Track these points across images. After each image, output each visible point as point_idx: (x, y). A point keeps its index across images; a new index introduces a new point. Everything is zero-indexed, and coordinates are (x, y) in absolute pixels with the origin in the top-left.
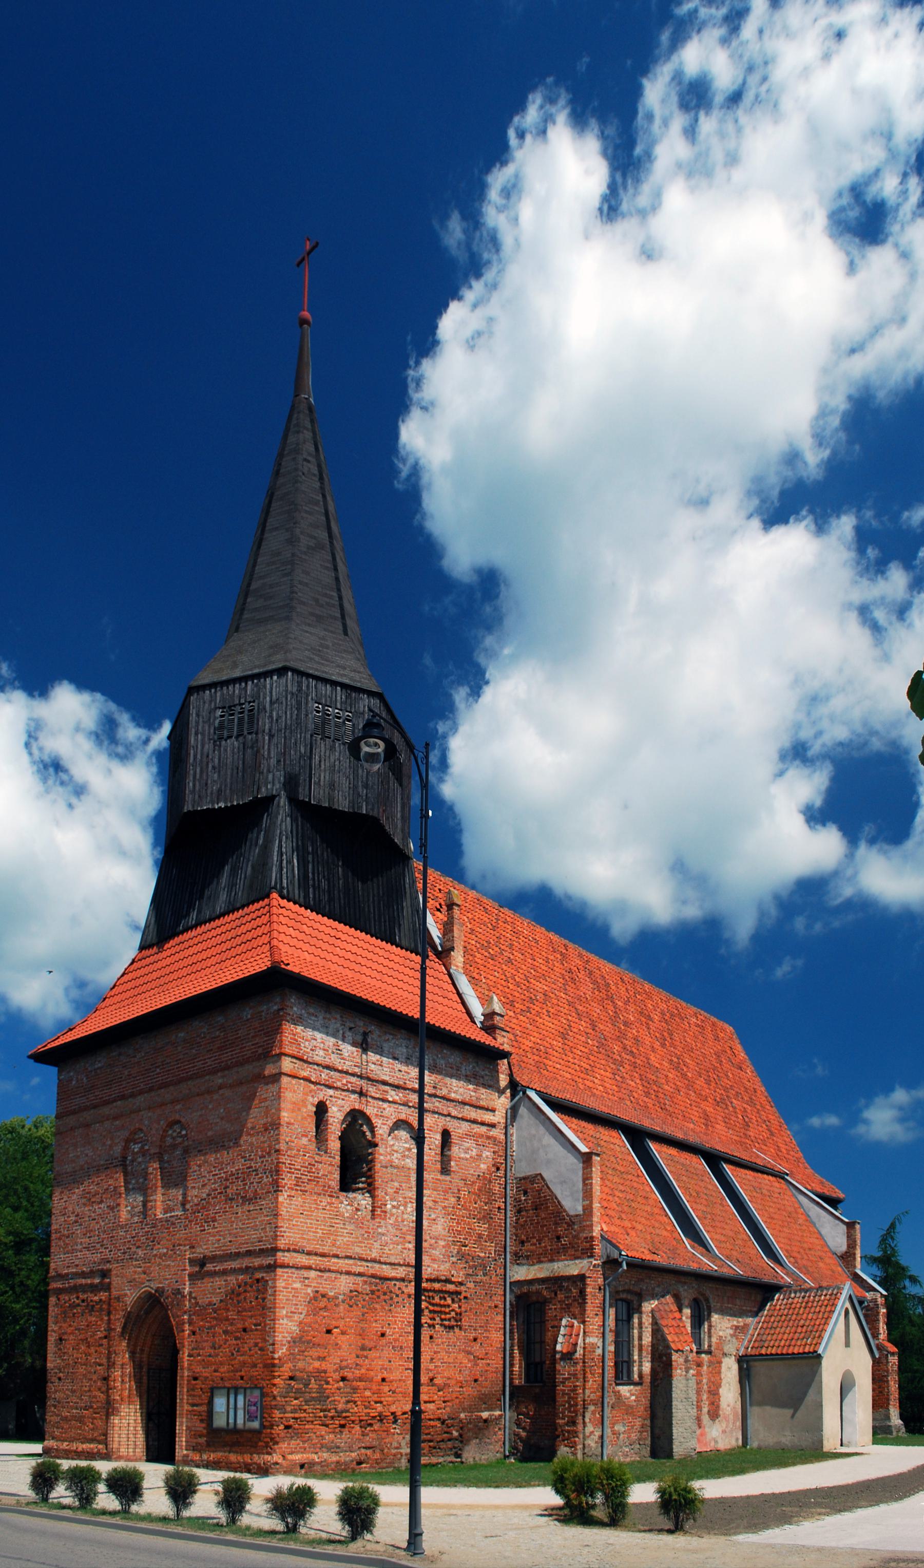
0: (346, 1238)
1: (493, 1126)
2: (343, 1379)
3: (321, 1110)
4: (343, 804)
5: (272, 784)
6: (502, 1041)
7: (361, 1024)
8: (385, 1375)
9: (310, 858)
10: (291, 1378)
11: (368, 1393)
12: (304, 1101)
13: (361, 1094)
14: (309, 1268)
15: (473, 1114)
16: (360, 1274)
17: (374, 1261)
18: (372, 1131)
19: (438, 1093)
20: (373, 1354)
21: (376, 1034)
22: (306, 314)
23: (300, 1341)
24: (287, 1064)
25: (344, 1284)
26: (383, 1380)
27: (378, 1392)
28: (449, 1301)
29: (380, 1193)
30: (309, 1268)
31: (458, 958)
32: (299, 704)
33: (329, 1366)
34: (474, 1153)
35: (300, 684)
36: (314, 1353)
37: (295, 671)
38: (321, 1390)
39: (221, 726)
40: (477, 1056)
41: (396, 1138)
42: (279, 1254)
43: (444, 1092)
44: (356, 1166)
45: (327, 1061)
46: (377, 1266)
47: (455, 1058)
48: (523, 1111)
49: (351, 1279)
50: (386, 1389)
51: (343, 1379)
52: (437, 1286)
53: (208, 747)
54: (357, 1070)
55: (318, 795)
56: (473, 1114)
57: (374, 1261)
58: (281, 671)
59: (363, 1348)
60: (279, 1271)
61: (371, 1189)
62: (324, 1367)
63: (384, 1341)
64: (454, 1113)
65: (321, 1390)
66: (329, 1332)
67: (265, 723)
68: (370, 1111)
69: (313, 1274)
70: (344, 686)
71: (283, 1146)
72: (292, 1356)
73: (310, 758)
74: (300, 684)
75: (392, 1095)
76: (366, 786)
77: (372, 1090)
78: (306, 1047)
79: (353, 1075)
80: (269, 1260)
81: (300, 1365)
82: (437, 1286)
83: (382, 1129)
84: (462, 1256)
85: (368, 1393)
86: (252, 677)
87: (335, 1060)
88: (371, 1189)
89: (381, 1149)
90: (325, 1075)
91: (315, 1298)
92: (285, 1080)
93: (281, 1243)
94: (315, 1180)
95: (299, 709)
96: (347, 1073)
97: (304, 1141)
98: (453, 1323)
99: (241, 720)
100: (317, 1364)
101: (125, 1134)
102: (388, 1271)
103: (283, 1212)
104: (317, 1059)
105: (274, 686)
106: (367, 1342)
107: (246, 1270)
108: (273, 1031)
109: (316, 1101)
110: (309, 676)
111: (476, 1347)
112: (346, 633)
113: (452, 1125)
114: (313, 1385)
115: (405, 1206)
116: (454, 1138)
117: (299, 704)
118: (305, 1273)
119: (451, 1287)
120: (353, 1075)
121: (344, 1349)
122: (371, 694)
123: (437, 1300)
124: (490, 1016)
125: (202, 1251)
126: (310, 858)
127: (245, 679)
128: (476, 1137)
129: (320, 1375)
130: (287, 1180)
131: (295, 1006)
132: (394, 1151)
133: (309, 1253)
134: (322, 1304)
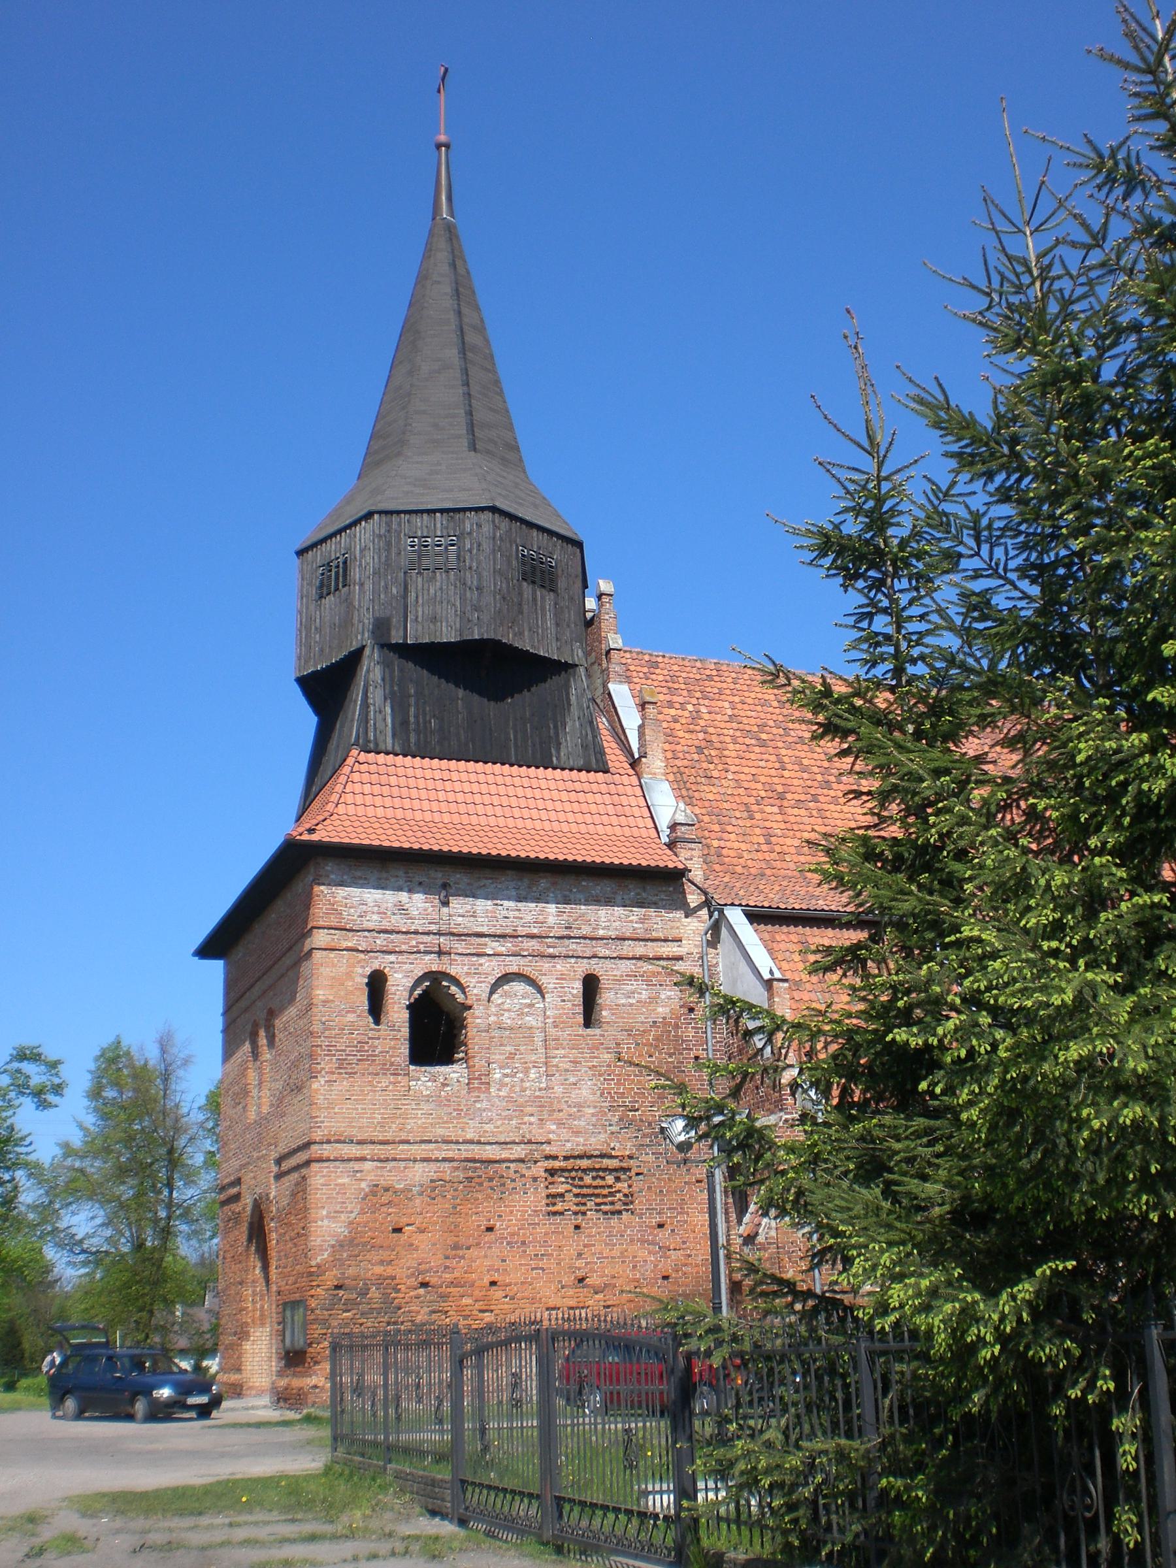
0: (418, 1120)
1: (679, 958)
2: (424, 1285)
3: (377, 985)
4: (448, 635)
5: (361, 636)
6: (692, 860)
7: (438, 876)
8: (496, 1277)
9: (412, 701)
10: (338, 1287)
11: (466, 1301)
12: (349, 975)
13: (440, 953)
14: (363, 1159)
15: (640, 949)
16: (444, 1160)
17: (471, 1142)
18: (463, 989)
19: (575, 933)
20: (474, 1252)
21: (459, 878)
22: (443, 138)
23: (352, 1244)
24: (320, 938)
25: (420, 1173)
26: (493, 1283)
27: (485, 1298)
28: (610, 1179)
29: (479, 1062)
30: (363, 1159)
31: (655, 763)
32: (389, 544)
33: (402, 1270)
34: (644, 995)
35: (389, 524)
36: (375, 1256)
37: (380, 513)
38: (387, 1301)
39: (321, 586)
40: (657, 884)
41: (506, 995)
42: (314, 1147)
43: (586, 930)
44: (437, 1030)
45: (386, 925)
46: (476, 1147)
47: (605, 887)
48: (724, 932)
49: (433, 1166)
50: (497, 1293)
51: (424, 1285)
52: (585, 1163)
53: (312, 607)
54: (434, 928)
55: (416, 633)
56: (640, 949)
57: (471, 1142)
58: (369, 516)
59: (456, 1247)
60: (315, 1166)
61: (466, 1060)
62: (390, 1271)
63: (489, 1237)
64: (603, 952)
65: (387, 1301)
66: (398, 1230)
67: (356, 574)
68: (453, 971)
69: (368, 1165)
70: (442, 511)
71: (317, 1027)
72: (336, 1261)
73: (405, 596)
74: (389, 524)
75: (492, 946)
76: (476, 608)
77: (460, 947)
78: (350, 916)
79: (428, 933)
80: (302, 1157)
81: (351, 1272)
82: (585, 1163)
83: (477, 989)
84: (626, 1123)
85: (466, 1301)
86: (344, 529)
87: (398, 922)
88: (466, 1060)
89: (478, 1010)
90: (381, 941)
91: (374, 1193)
92: (317, 955)
93: (318, 1135)
94: (371, 1058)
95: (388, 550)
96: (416, 933)
97: (351, 1017)
98: (618, 1207)
99: (337, 573)
100: (378, 1270)
101: (249, 1028)
102: (491, 1152)
103: (320, 1100)
104: (370, 925)
105: (364, 532)
106: (462, 1240)
107: (297, 1168)
108: (307, 902)
109: (368, 971)
110: (398, 512)
111: (663, 1235)
112: (473, 447)
113: (597, 967)
114: (374, 1293)
115: (526, 1071)
116: (604, 983)
117: (389, 544)
118: (357, 1166)
119: (614, 1163)
120: (428, 933)
121: (424, 1249)
122: (478, 510)
123: (588, 1180)
124: (673, 827)
125: (282, 1148)
126: (412, 701)
127: (339, 532)
128: (647, 979)
129: (389, 1284)
130: (326, 1064)
131: (330, 866)
132: (488, 1015)
133: (360, 1143)
134: (385, 1199)
